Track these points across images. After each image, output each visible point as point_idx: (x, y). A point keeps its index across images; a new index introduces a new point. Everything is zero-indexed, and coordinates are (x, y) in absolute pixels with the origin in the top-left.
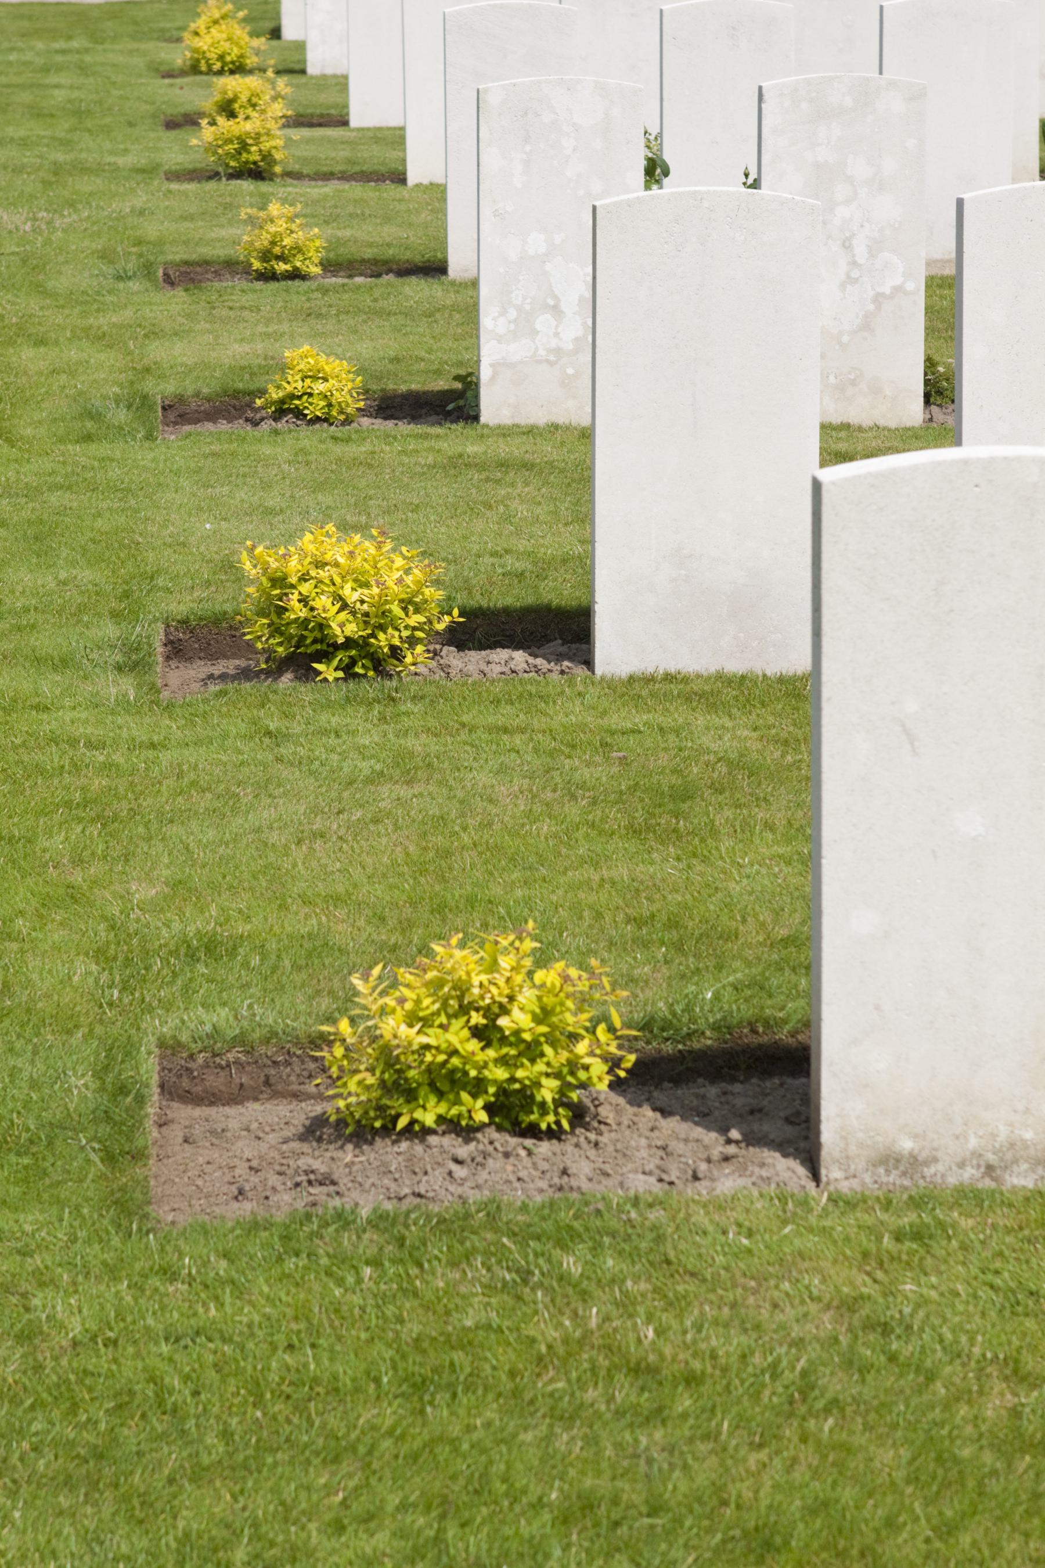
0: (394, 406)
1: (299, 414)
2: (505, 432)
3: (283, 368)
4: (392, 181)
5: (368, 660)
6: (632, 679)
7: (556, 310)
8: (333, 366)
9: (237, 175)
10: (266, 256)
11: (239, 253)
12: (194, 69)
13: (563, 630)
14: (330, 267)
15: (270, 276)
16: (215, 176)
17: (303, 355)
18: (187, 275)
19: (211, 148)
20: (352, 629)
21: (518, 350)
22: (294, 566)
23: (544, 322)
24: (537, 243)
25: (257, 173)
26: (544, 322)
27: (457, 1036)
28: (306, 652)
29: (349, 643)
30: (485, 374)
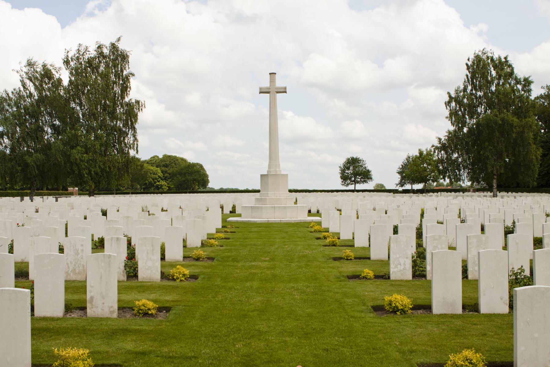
0: (377, 277)
1: (366, 278)
2: (141, 282)
3: (364, 272)
4: (197, 247)
5: (403, 312)
6: (440, 315)
7: (400, 265)
8: (370, 272)
9: (332, 246)
10: (347, 257)
11: (343, 256)
12: (315, 232)
13: (428, 308)
14: (355, 258)
15: (348, 260)
16: (329, 246)
17: (366, 270)
18: (335, 259)
19: (330, 242)
20: (402, 307)
21: (396, 270)
22: (393, 299)
23: (399, 266)
24: (398, 256)
25: (334, 245)
26: (399, 266)
27: (467, 363)
28: (395, 311)
29: (401, 309)
30: (391, 273)
